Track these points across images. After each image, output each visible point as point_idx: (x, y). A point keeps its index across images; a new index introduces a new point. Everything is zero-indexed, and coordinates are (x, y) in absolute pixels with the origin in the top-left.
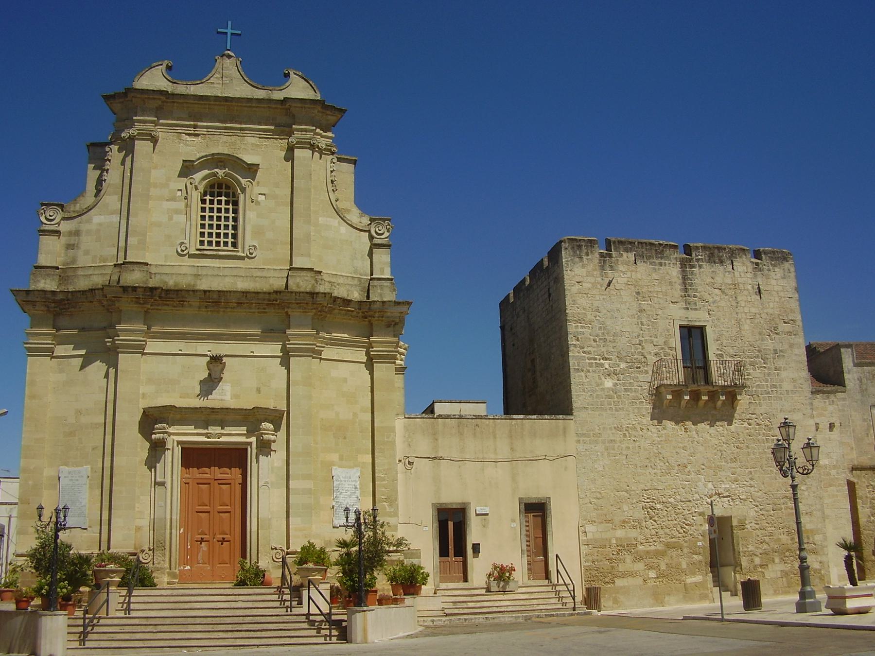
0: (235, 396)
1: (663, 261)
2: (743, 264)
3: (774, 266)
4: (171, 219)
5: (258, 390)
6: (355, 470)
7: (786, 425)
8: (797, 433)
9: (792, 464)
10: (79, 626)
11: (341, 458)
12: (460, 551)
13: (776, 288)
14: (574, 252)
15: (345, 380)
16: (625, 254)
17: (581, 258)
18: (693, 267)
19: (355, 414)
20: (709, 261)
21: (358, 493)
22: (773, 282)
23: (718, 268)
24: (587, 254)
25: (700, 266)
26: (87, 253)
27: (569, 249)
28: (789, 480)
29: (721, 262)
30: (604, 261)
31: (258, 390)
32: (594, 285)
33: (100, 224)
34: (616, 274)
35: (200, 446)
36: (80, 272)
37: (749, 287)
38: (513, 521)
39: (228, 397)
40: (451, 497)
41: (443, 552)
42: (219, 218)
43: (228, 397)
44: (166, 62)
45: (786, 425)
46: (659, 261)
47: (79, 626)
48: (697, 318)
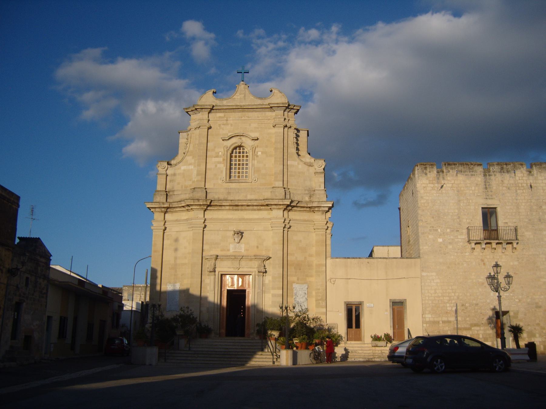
0: (247, 250)
1: (473, 173)
2: (522, 172)
3: (541, 172)
4: (216, 166)
5: (258, 247)
6: (305, 285)
7: (497, 266)
8: (502, 270)
9: (498, 284)
10: (269, 358)
11: (298, 279)
12: (358, 326)
13: (542, 185)
14: (423, 171)
15: (301, 241)
16: (451, 171)
17: (426, 174)
18: (489, 175)
19: (305, 258)
20: (500, 172)
21: (306, 296)
22: (540, 181)
23: (507, 176)
24: (430, 172)
25: (495, 175)
26: (179, 184)
27: (420, 170)
28: (497, 294)
29: (508, 172)
30: (439, 175)
31: (258, 247)
32: (433, 188)
33: (184, 170)
34: (446, 182)
35: (489, 223)
36: (175, 193)
37: (525, 185)
38: (386, 311)
39: (243, 251)
40: (354, 299)
41: (349, 326)
42: (239, 164)
43: (243, 251)
44: (213, 90)
45: (497, 266)
46: (471, 173)
47: (269, 358)
48: (491, 203)
